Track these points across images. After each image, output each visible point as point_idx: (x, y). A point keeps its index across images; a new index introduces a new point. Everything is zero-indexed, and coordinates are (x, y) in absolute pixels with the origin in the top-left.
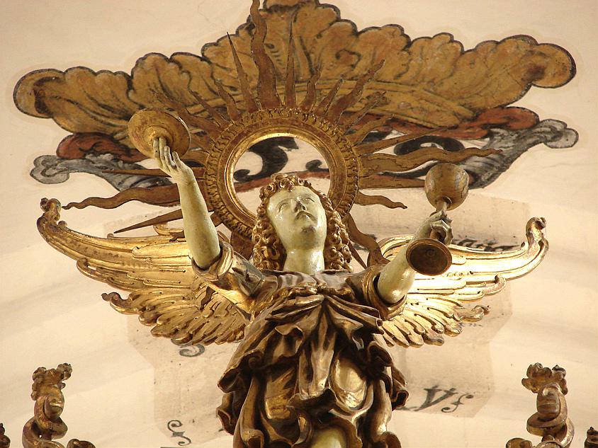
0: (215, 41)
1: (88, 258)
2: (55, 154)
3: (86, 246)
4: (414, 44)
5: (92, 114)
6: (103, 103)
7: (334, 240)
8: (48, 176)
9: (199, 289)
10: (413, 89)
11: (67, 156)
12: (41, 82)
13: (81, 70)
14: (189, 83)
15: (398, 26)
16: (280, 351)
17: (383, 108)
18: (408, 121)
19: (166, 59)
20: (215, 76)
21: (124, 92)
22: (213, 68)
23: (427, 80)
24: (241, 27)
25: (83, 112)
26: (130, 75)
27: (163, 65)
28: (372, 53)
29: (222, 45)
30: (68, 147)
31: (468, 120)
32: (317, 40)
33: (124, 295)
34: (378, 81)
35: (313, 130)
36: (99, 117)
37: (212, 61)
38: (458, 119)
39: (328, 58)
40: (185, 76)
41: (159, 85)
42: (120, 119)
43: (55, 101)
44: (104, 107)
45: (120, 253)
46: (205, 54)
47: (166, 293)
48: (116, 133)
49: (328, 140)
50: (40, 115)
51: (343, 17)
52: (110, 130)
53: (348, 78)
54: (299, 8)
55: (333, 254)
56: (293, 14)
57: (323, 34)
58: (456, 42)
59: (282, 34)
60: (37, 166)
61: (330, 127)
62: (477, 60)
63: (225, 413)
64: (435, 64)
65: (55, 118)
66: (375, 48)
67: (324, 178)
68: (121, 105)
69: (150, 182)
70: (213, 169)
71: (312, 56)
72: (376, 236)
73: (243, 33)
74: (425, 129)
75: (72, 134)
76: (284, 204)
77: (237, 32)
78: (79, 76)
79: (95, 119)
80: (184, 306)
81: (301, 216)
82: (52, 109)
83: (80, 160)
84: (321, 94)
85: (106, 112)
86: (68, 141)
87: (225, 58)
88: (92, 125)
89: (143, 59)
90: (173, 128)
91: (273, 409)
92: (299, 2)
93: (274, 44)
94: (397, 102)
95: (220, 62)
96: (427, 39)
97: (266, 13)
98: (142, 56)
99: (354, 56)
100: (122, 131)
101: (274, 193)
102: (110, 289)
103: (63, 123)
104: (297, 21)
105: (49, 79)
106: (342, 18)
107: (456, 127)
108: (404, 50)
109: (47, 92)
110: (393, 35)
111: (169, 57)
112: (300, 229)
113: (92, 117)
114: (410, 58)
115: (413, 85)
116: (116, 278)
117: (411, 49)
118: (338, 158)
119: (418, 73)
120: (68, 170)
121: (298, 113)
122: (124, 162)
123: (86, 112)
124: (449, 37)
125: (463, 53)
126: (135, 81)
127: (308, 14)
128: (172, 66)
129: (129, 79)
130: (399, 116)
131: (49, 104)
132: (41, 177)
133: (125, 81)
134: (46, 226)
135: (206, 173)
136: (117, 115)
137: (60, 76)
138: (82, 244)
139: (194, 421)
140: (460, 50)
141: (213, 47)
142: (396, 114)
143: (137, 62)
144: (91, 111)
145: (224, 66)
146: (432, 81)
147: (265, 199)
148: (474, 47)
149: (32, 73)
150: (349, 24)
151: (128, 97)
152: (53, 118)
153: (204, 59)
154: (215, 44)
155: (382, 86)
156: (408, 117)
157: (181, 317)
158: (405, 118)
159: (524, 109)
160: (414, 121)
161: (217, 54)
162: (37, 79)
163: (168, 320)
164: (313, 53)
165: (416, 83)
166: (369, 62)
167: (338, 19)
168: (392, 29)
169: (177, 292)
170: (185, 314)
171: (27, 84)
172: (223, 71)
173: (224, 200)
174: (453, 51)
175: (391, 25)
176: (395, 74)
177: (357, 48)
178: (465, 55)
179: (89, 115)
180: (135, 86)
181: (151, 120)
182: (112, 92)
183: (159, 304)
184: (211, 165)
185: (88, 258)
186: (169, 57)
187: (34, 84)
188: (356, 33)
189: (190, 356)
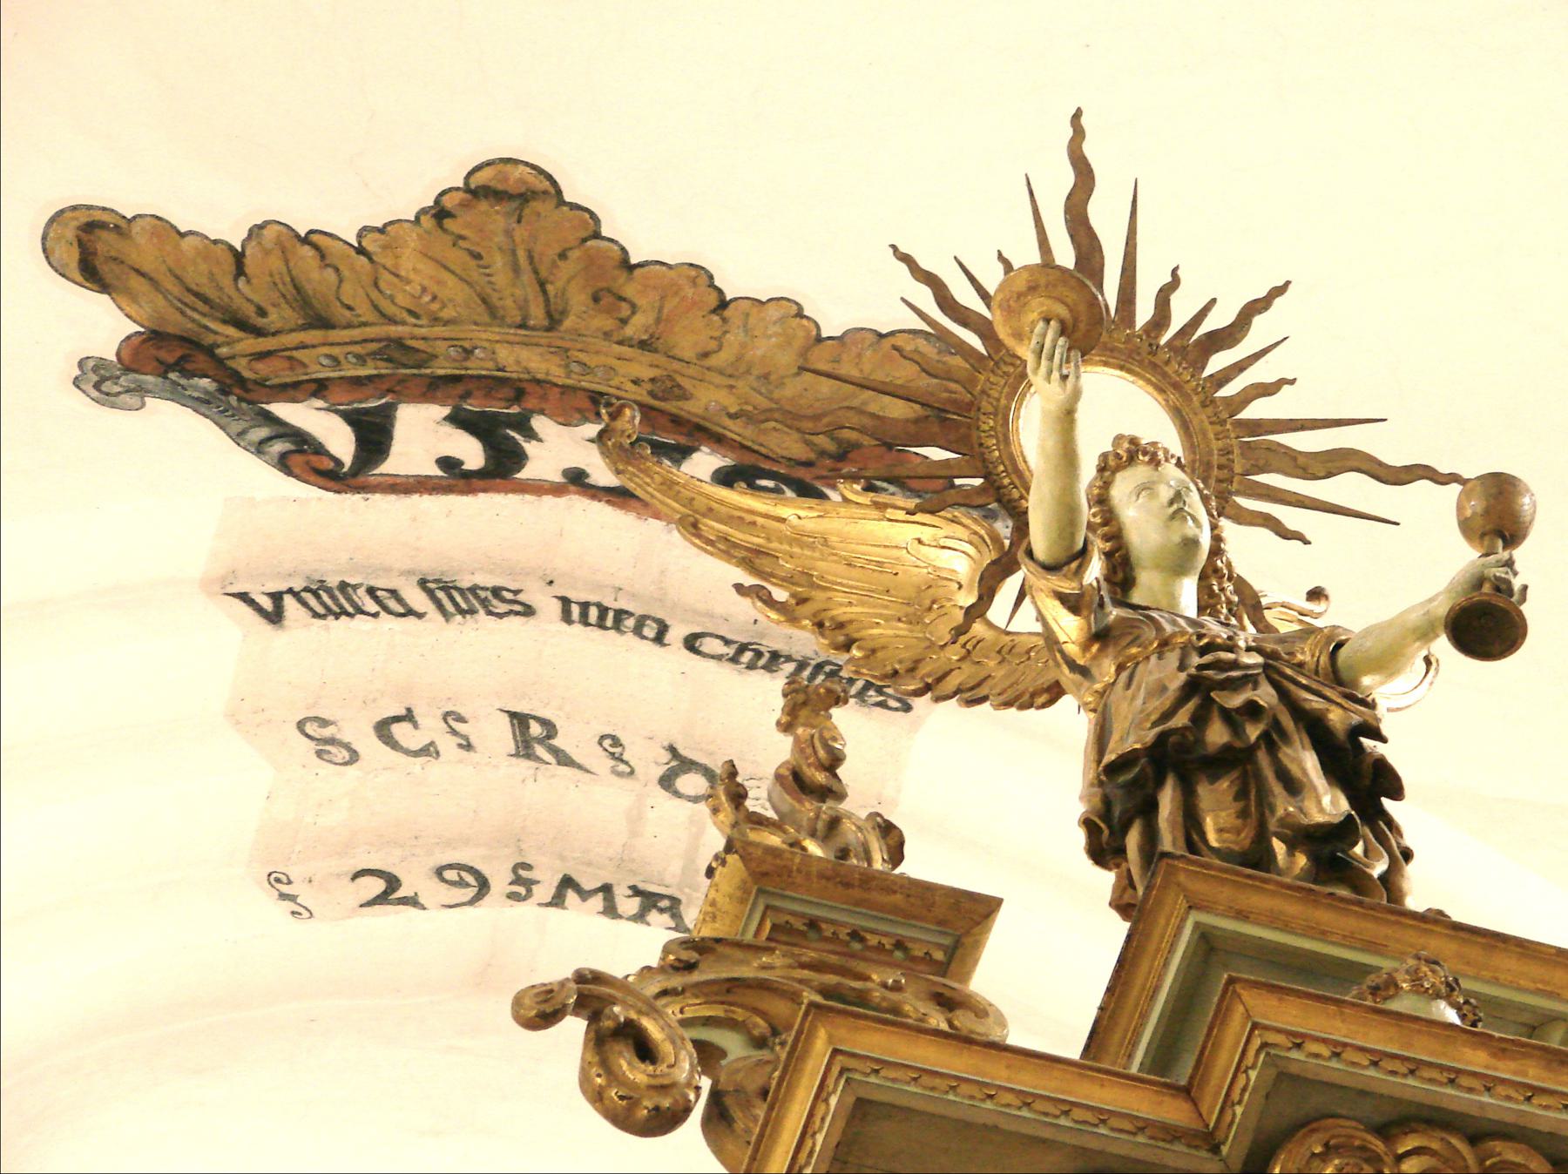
0: (379, 224)
1: (698, 516)
2: (114, 359)
3: (693, 495)
4: (732, 306)
5: (175, 302)
6: (194, 287)
7: (1216, 570)
8: (107, 394)
9: (930, 609)
10: (732, 382)
11: (134, 366)
12: (91, 227)
13: (159, 223)
14: (339, 287)
15: (703, 268)
16: (1217, 735)
17: (680, 404)
18: (724, 436)
19: (297, 236)
20: (382, 285)
21: (230, 277)
22: (376, 272)
23: (756, 372)
24: (423, 211)
25: (160, 296)
26: (240, 249)
27: (294, 247)
28: (657, 305)
29: (392, 234)
30: (136, 352)
31: (831, 456)
32: (559, 263)
33: (780, 595)
34: (669, 357)
35: (1165, 375)
36: (189, 312)
37: (375, 258)
38: (812, 450)
39: (578, 300)
40: (330, 274)
41: (288, 279)
42: (225, 322)
43: (113, 266)
44: (197, 295)
45: (760, 520)
46: (364, 244)
47: (862, 604)
48: (219, 346)
49: (1187, 398)
50: (88, 285)
51: (605, 232)
52: (209, 339)
53: (615, 339)
54: (527, 201)
55: (1212, 594)
56: (516, 209)
57: (570, 254)
58: (807, 318)
59: (496, 239)
60: (84, 373)
61: (1192, 376)
62: (845, 357)
63: (1098, 822)
64: (766, 347)
65: (114, 295)
66: (663, 298)
67: (600, 501)
68: (226, 299)
69: (293, 443)
70: (992, 404)
71: (549, 288)
72: (668, 623)
73: (427, 222)
74: (757, 456)
75: (142, 330)
76: (1146, 488)
77: (417, 218)
78: (155, 233)
79: (183, 313)
80: (901, 633)
81: (1178, 516)
82: (109, 279)
83: (160, 380)
84: (568, 357)
85: (200, 305)
86: (136, 340)
87: (397, 257)
88: (176, 323)
89: (261, 227)
90: (1082, 308)
91: (1220, 831)
92: (527, 190)
93: (483, 254)
94: (704, 401)
95: (389, 262)
96: (757, 304)
97: (468, 196)
98: (259, 222)
99: (624, 304)
100: (228, 344)
101: (1125, 468)
102: (749, 580)
103: (128, 308)
104: (523, 220)
105: (103, 225)
106: (603, 234)
107: (808, 464)
108: (714, 311)
109: (100, 247)
110: (694, 281)
111: (303, 235)
112: (1176, 538)
113: (178, 309)
114: (724, 329)
115: (730, 376)
116: (757, 561)
117: (727, 313)
118: (1204, 433)
119: (739, 358)
120: (141, 391)
121: (1141, 339)
122: (240, 399)
123: (165, 298)
124: (795, 307)
125: (819, 339)
126: (250, 263)
127: (543, 214)
128: (307, 251)
129: (239, 257)
130: (708, 425)
131: (105, 269)
132: (95, 394)
133: (230, 259)
134: (614, 445)
135: (979, 409)
136: (221, 316)
137: (122, 223)
138: (682, 490)
139: (310, 881)
140: (814, 333)
141: (377, 235)
142: (704, 419)
143: (251, 230)
144: (175, 297)
145: (393, 270)
146: (766, 376)
147: (1107, 474)
148: (839, 335)
149: (74, 208)
150: (616, 248)
151: (238, 289)
152: (109, 294)
153: (361, 251)
154: (381, 230)
155: (676, 365)
156: (725, 428)
157: (897, 652)
158: (721, 430)
159: (927, 458)
160: (738, 438)
161: (385, 247)
162: (84, 220)
163: (874, 651)
164: (552, 283)
165: (736, 373)
166: (651, 321)
167: (597, 235)
168: (693, 273)
169: (886, 607)
170: (907, 648)
171: (67, 225)
172: (395, 280)
173: (1007, 463)
174: (801, 334)
175: (691, 265)
176: (699, 350)
177: (629, 291)
178: (821, 346)
179: (172, 305)
180: (247, 270)
181: (1047, 286)
182: (211, 274)
183: (851, 622)
184: (989, 396)
185: (698, 516)
186: (303, 235)
187: (79, 228)
188: (627, 266)
189: (336, 764)
